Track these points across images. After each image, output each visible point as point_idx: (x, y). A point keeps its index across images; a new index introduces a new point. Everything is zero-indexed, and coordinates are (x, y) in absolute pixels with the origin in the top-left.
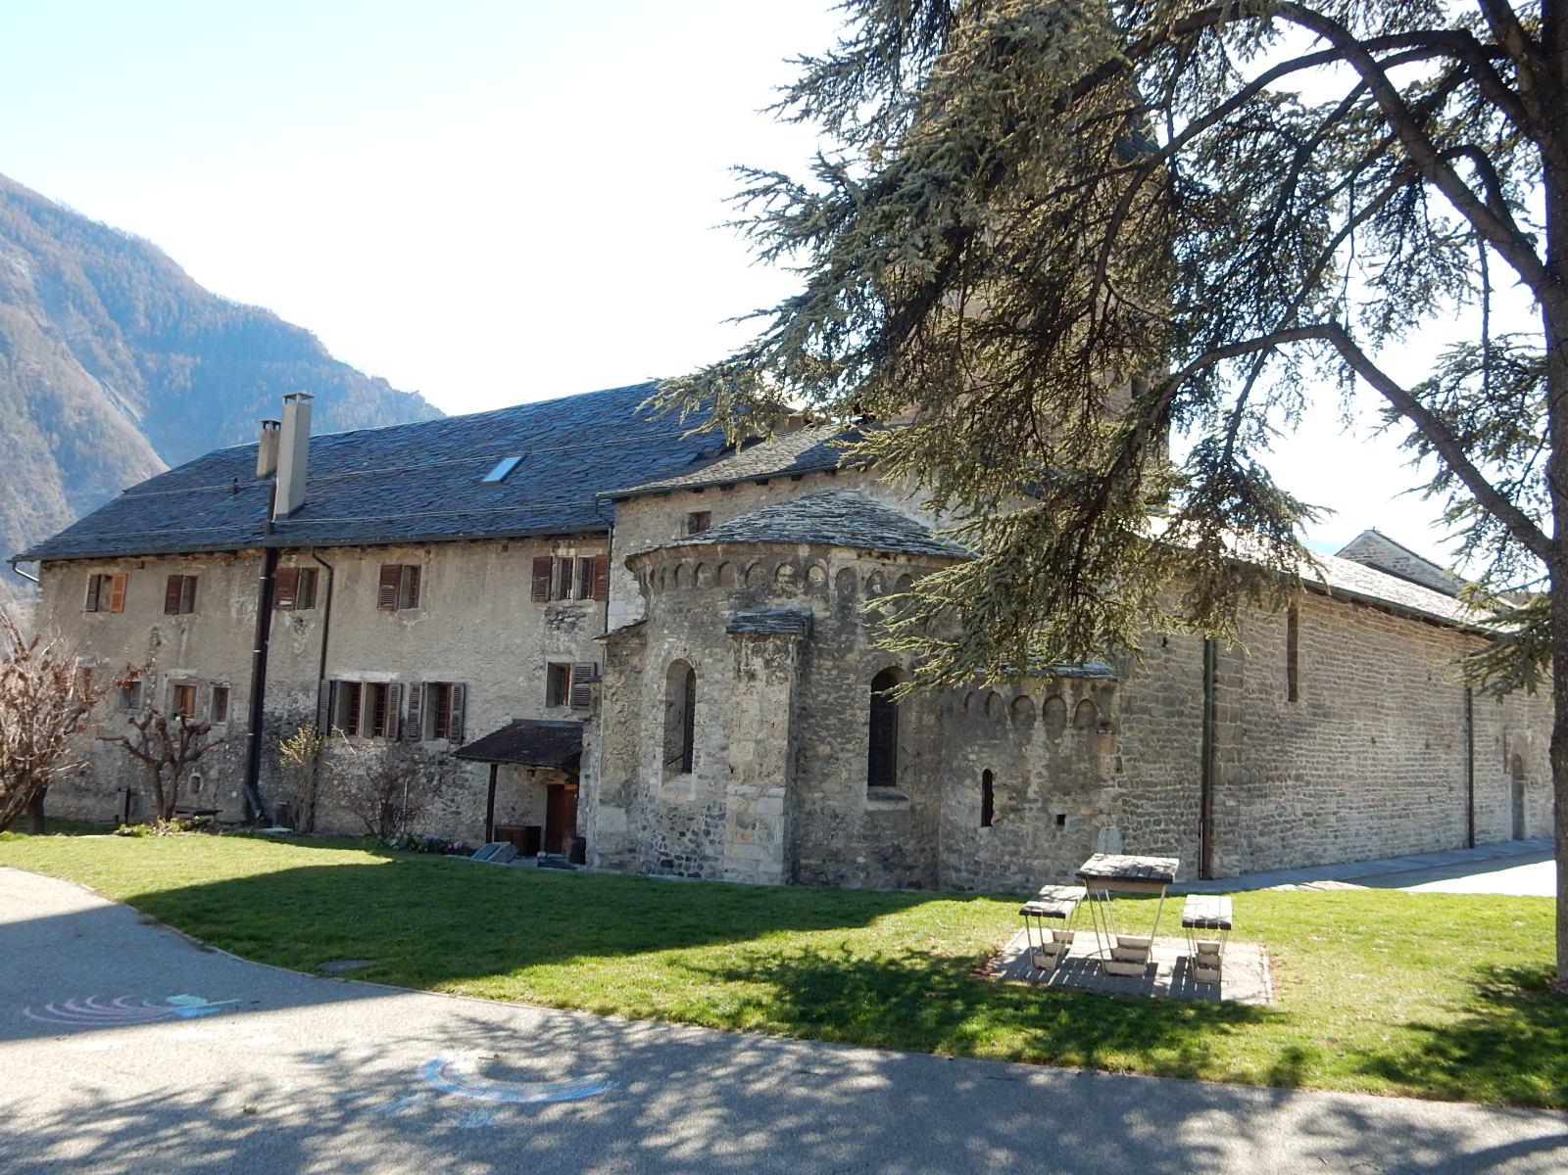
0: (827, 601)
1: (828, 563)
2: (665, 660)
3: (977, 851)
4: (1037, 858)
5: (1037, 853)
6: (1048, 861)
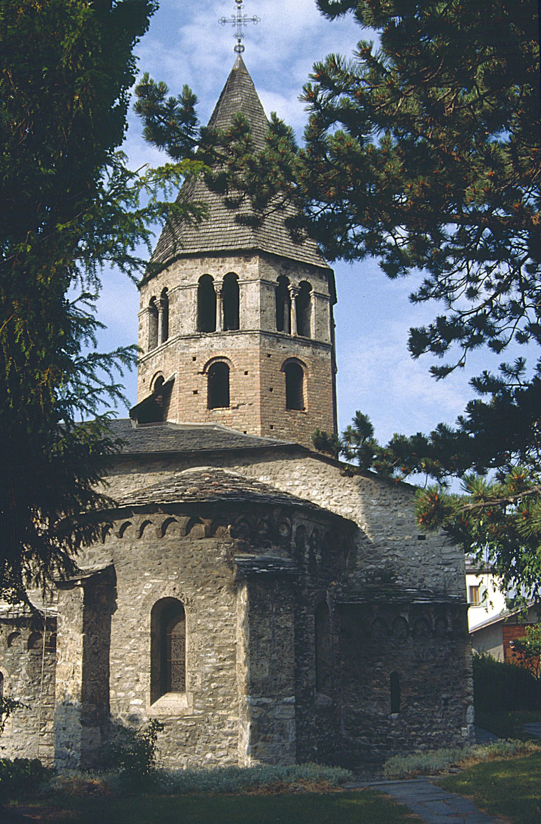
0: (289, 551)
1: (292, 521)
2: (148, 598)
3: (389, 731)
4: (435, 730)
5: (434, 727)
6: (441, 732)
